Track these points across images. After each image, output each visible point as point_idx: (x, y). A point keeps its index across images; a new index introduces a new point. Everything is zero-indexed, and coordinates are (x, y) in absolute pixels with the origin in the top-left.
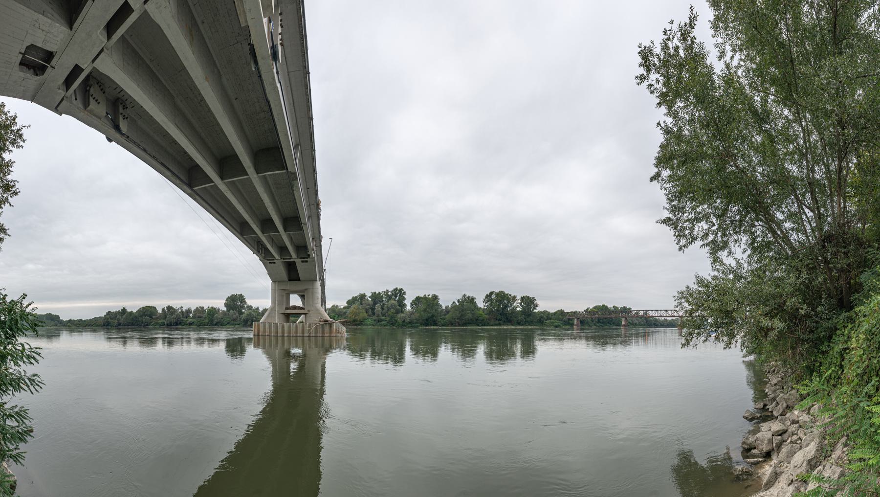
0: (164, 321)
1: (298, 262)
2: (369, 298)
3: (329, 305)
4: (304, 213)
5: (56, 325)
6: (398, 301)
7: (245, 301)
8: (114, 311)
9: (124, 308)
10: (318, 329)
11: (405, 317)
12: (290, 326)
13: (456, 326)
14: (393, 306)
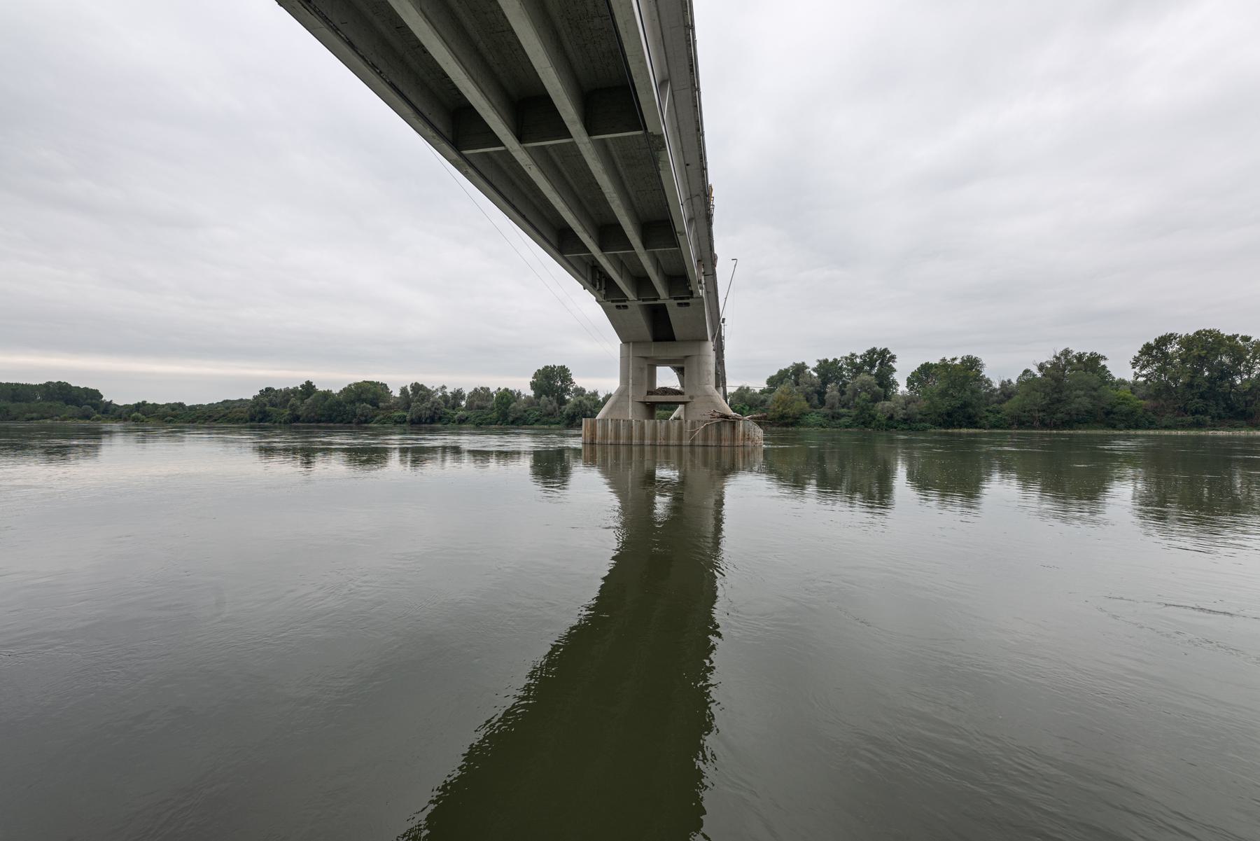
0: (405, 414)
1: (671, 305)
2: (812, 372)
3: (732, 387)
4: (682, 212)
5: (88, 417)
6: (876, 375)
7: (571, 380)
9: (308, 383)
11: (893, 409)
12: (655, 426)
13: (1034, 428)
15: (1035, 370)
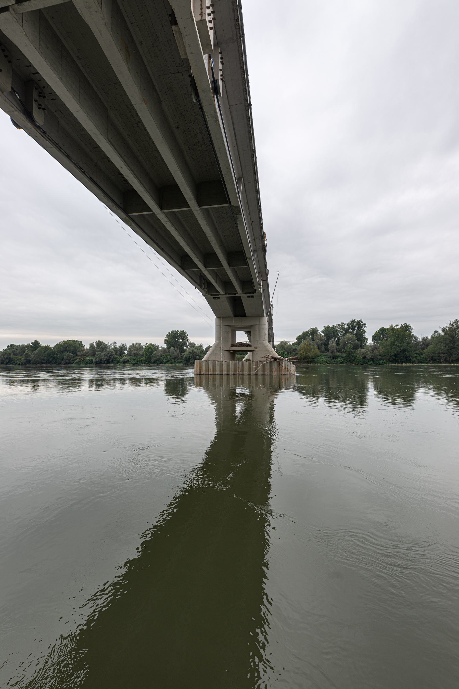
0: (92, 358)
1: (244, 297)
2: (321, 333)
3: (277, 341)
6: (356, 334)
7: (187, 338)
8: (21, 344)
10: (266, 367)
11: (366, 353)
12: (235, 364)
13: (441, 363)
14: (349, 341)
15: (440, 331)
